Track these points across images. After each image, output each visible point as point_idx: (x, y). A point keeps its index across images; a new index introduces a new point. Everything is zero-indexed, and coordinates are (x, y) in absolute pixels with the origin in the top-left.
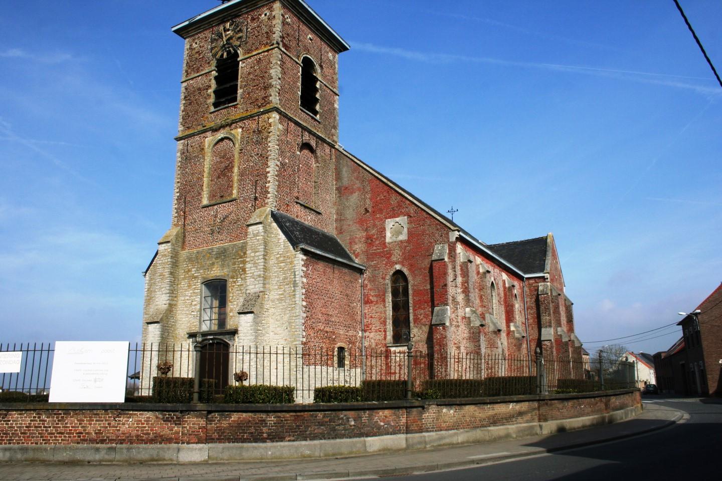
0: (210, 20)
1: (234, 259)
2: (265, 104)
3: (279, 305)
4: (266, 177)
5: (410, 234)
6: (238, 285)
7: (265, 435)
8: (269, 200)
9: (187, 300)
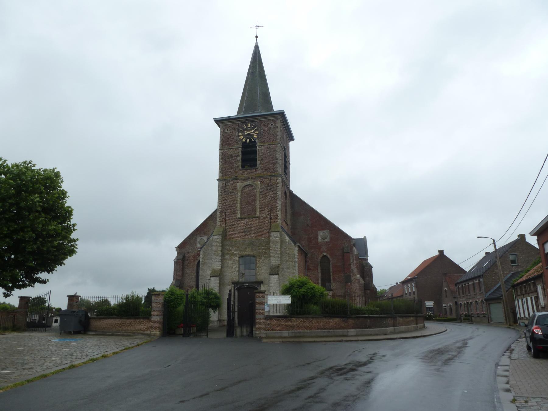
0: (238, 120)
1: (259, 247)
2: (274, 172)
4: (277, 209)
5: (331, 239)
6: (262, 260)
7: (368, 326)
8: (279, 220)
9: (230, 265)
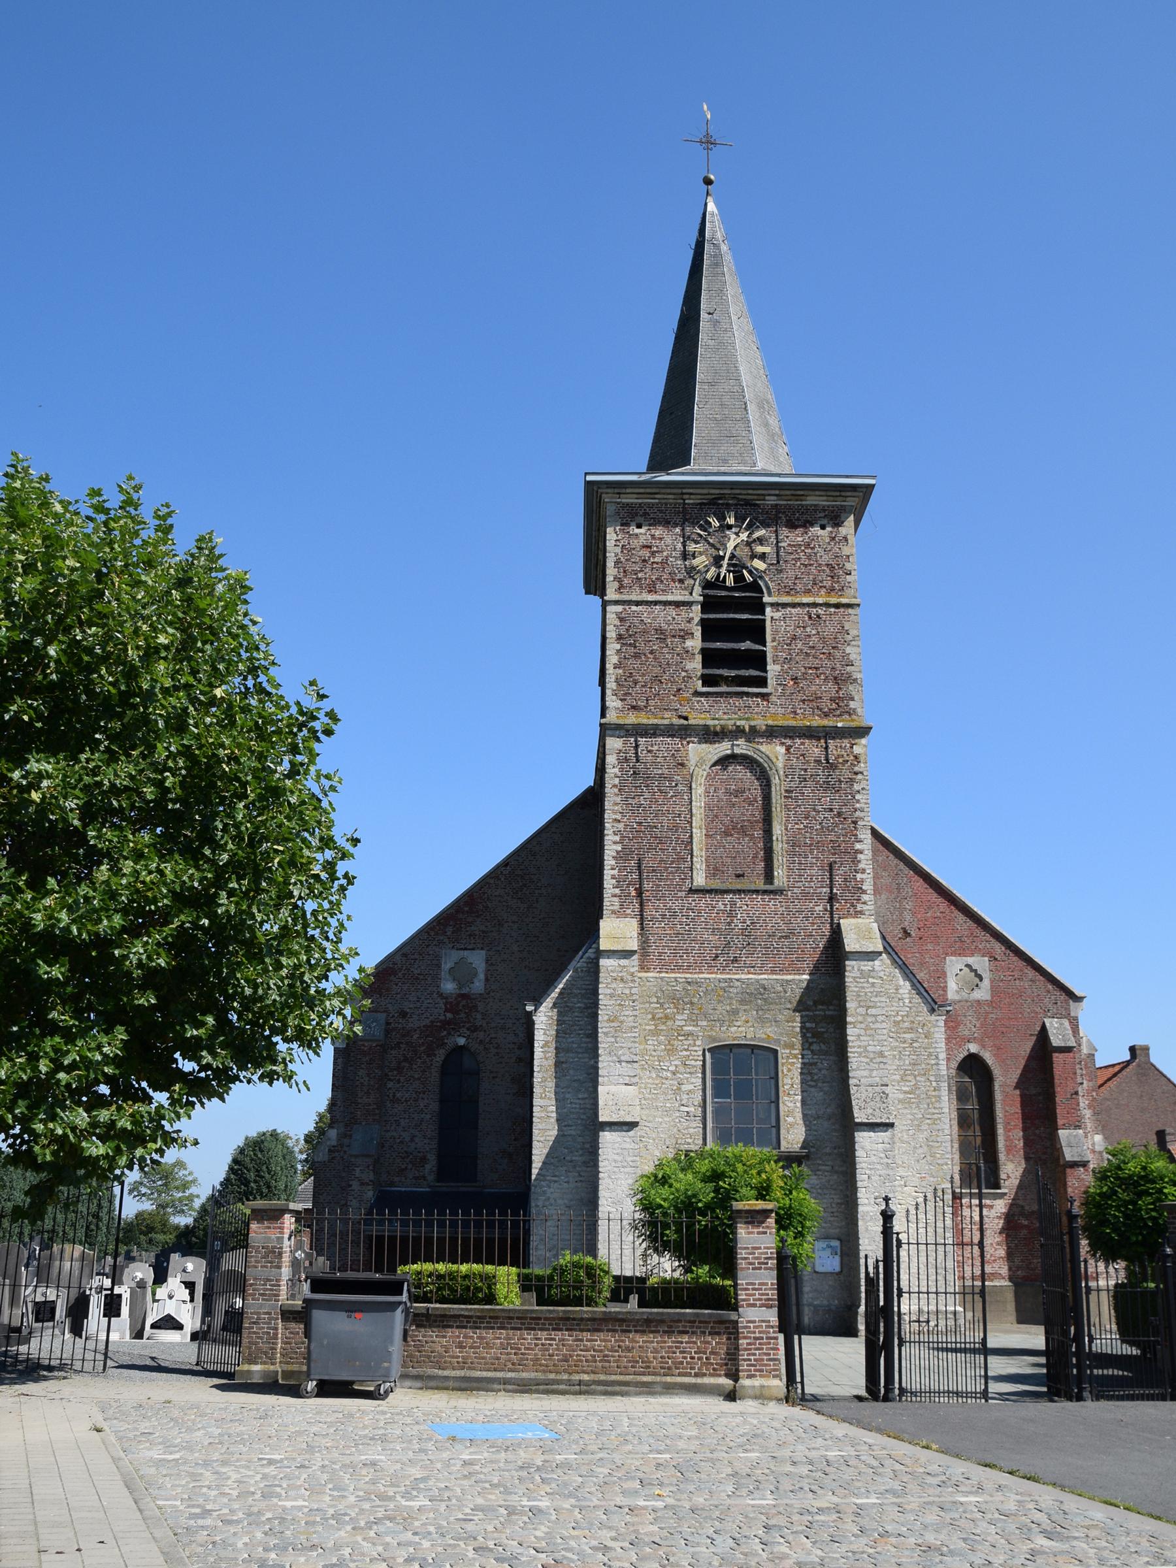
0: (684, 491)
2: (838, 712)
3: (905, 1111)
4: (855, 861)
8: (865, 907)
